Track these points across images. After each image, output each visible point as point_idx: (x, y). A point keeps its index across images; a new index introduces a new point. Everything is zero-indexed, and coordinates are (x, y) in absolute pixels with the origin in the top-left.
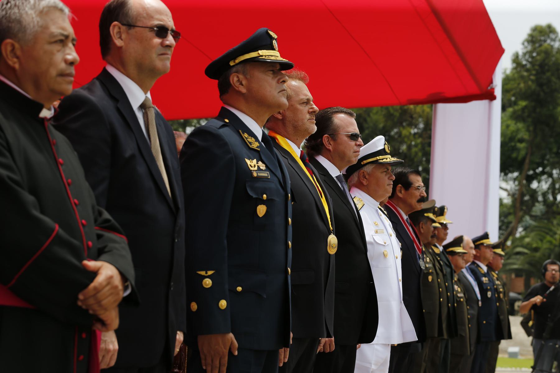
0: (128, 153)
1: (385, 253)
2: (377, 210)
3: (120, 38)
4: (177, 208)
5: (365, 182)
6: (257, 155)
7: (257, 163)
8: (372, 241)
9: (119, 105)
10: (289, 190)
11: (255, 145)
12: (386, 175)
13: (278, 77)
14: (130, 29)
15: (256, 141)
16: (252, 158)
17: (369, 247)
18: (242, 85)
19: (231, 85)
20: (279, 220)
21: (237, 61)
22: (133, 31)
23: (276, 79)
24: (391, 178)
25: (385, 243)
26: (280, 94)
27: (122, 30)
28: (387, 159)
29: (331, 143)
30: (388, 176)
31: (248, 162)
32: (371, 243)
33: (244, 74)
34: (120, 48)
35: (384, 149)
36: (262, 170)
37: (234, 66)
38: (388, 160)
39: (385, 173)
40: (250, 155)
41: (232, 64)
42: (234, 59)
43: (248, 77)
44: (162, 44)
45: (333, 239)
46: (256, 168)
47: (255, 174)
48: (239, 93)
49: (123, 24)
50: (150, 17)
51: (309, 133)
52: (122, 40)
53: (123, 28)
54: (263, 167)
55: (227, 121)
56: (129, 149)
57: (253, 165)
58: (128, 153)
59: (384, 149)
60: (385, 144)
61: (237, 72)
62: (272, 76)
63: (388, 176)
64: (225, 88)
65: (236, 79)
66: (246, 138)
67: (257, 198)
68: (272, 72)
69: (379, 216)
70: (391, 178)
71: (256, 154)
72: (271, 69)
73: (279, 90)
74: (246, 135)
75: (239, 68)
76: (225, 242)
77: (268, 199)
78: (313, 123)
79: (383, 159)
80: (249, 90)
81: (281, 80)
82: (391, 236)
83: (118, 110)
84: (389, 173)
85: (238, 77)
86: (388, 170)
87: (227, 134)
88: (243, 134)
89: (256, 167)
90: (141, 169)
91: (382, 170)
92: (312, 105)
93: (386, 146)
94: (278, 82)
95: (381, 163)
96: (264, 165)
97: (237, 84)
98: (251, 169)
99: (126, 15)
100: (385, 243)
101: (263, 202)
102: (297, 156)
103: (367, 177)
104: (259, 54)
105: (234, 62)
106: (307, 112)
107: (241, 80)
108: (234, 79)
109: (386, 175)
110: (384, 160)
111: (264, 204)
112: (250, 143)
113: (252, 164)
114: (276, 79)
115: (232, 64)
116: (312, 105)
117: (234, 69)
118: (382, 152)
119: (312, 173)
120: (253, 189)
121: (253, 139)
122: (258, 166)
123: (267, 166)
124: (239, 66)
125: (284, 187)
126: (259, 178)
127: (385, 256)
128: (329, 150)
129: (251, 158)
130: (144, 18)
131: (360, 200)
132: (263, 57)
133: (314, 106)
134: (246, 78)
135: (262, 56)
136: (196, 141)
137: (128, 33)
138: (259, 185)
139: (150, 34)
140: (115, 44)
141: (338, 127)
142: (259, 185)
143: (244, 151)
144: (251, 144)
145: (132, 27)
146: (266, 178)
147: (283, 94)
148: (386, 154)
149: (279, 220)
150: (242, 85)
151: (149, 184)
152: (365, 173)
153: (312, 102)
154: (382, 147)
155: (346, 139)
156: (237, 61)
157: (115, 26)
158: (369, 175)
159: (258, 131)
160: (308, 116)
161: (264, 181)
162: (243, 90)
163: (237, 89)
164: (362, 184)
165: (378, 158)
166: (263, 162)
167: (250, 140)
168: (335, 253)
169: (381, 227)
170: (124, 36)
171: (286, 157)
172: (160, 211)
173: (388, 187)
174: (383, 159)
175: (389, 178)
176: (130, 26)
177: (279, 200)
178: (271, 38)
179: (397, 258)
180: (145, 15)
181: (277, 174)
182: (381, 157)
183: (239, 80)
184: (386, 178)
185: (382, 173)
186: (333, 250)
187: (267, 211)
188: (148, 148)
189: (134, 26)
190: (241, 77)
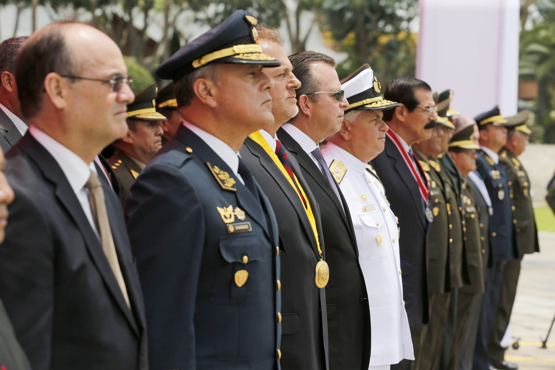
0: (75, 265)
1: (379, 238)
2: (364, 175)
3: (59, 94)
4: (141, 328)
5: (346, 136)
6: (234, 198)
7: (234, 211)
8: (360, 223)
9: (58, 193)
10: (277, 241)
11: (229, 184)
12: (376, 124)
13: (261, 82)
14: (73, 82)
15: (230, 177)
16: (227, 203)
17: (357, 233)
18: (211, 95)
19: (194, 94)
20: (265, 287)
21: (204, 61)
22: (78, 85)
23: (258, 85)
24: (383, 129)
25: (378, 225)
26: (264, 106)
27: (61, 84)
28: (377, 102)
29: (310, 105)
30: (380, 125)
31: (221, 210)
32: (360, 228)
33: (214, 79)
34: (59, 111)
35: (373, 88)
36: (240, 221)
37: (198, 68)
38: (379, 105)
39: (375, 122)
40: (224, 199)
41: (196, 64)
42: (200, 58)
43: (219, 84)
44: (118, 100)
45: (322, 267)
46: (232, 220)
47: (231, 229)
48: (207, 107)
49: (63, 76)
50: (100, 63)
51: (288, 117)
52: (62, 97)
53: (64, 81)
54: (241, 215)
55: (189, 150)
56: (77, 258)
57: (228, 216)
58: (75, 265)
59: (373, 88)
60: (374, 81)
61: (203, 77)
62: (251, 81)
63: (380, 125)
64: (186, 97)
65: (201, 87)
66: (217, 174)
67: (234, 263)
68: (251, 76)
69: (367, 182)
70: (383, 129)
71: (232, 197)
72: (251, 71)
73: (262, 102)
74: (216, 170)
75: (206, 70)
76: (192, 328)
77: (249, 262)
78: (293, 103)
79: (371, 103)
80: (221, 101)
81: (265, 87)
82: (384, 211)
83: (58, 200)
84: (379, 122)
85: (204, 84)
86: (378, 117)
87: (192, 173)
88: (213, 167)
89: (233, 217)
90: (94, 280)
91: (369, 119)
92: (291, 77)
93: (376, 84)
94: (260, 89)
95: (369, 110)
96: (243, 213)
97: (204, 94)
98: (226, 221)
99: (67, 62)
100: (378, 225)
101: (242, 266)
102: (272, 150)
103: (349, 128)
104: (234, 51)
105: (199, 62)
106: (285, 87)
107: (208, 88)
108: (199, 87)
109: (376, 124)
110: (374, 105)
111: (244, 269)
112: (223, 181)
113: (229, 215)
114: (258, 85)
115: (196, 64)
116: (291, 77)
117: (199, 73)
118: (371, 93)
119: (291, 170)
120: (229, 249)
121: (227, 175)
122: (235, 216)
123: (247, 214)
124: (205, 68)
125: (270, 239)
126: (237, 234)
127: (378, 242)
128: (307, 116)
129: (224, 206)
130: (93, 65)
131: (341, 165)
132: (240, 56)
133: (295, 79)
134: (216, 86)
135: (238, 54)
136: (149, 185)
137: (70, 88)
138: (237, 243)
139: (103, 88)
140: (53, 105)
141: (319, 83)
142: (237, 243)
143: (216, 193)
144: (224, 183)
145: (77, 80)
146: (245, 231)
147: (268, 106)
148: (376, 95)
149: (265, 287)
150: (211, 95)
151: (103, 300)
152: (347, 124)
153: (291, 74)
154: (370, 86)
155: (330, 99)
156: (204, 61)
157: (51, 79)
158: (352, 125)
159: (233, 162)
160: (286, 94)
161: (246, 236)
162: (212, 103)
163: (203, 101)
164: (342, 138)
165: (365, 102)
166: (242, 209)
167: (222, 177)
168: (326, 287)
169: (372, 201)
170: (64, 92)
171: (257, 154)
172: (115, 335)
173: (378, 142)
174: (371, 103)
175: (380, 129)
176: (73, 78)
177: (264, 260)
178: (250, 25)
179: (394, 242)
180: (93, 61)
181: (262, 224)
182: (368, 101)
183: (206, 88)
184: (377, 128)
185: (371, 122)
186: (322, 282)
187: (249, 279)
188: (99, 246)
189: (80, 78)
190: (209, 83)
